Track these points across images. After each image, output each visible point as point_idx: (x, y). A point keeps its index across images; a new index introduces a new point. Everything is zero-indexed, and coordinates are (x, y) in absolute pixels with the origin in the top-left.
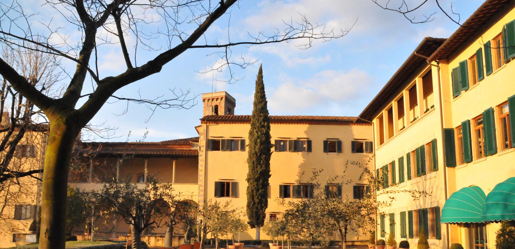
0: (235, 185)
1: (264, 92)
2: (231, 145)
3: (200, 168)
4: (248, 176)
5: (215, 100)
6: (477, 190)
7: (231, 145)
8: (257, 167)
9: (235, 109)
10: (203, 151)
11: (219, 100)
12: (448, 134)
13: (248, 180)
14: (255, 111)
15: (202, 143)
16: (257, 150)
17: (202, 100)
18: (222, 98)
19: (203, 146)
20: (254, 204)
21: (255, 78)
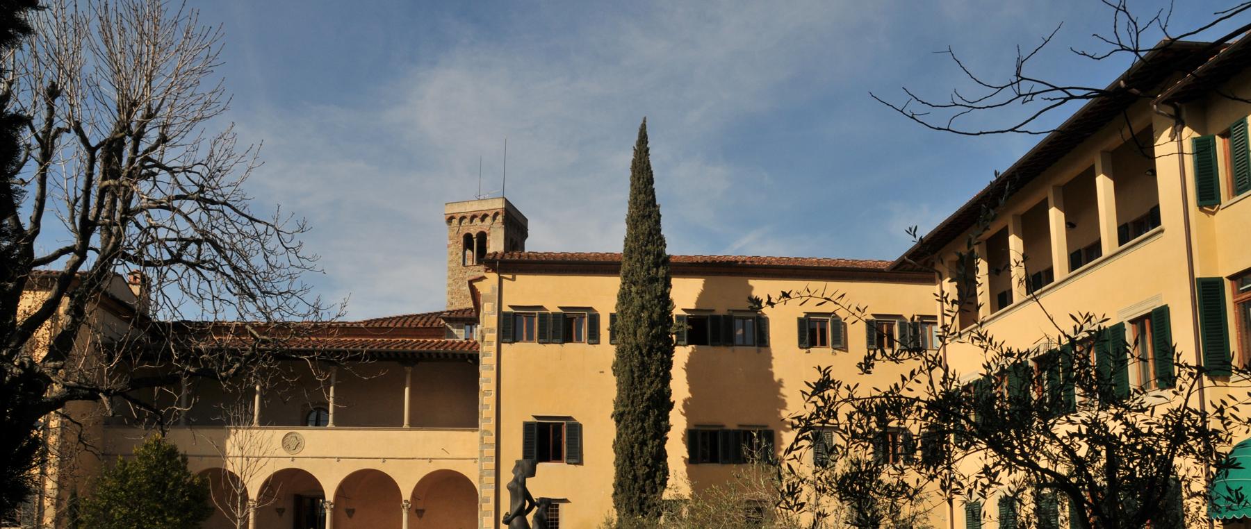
0: (576, 430)
1: (652, 191)
2: (564, 327)
3: (483, 386)
4: (616, 406)
5: (466, 221)
6: (518, 462)
7: (564, 327)
8: (641, 383)
9: (527, 242)
10: (490, 343)
11: (488, 220)
12: (1208, 294)
13: (619, 417)
14: (631, 239)
15: (489, 319)
16: (641, 340)
17: (444, 220)
18: (497, 214)
19: (491, 331)
20: (635, 478)
21: (628, 157)
